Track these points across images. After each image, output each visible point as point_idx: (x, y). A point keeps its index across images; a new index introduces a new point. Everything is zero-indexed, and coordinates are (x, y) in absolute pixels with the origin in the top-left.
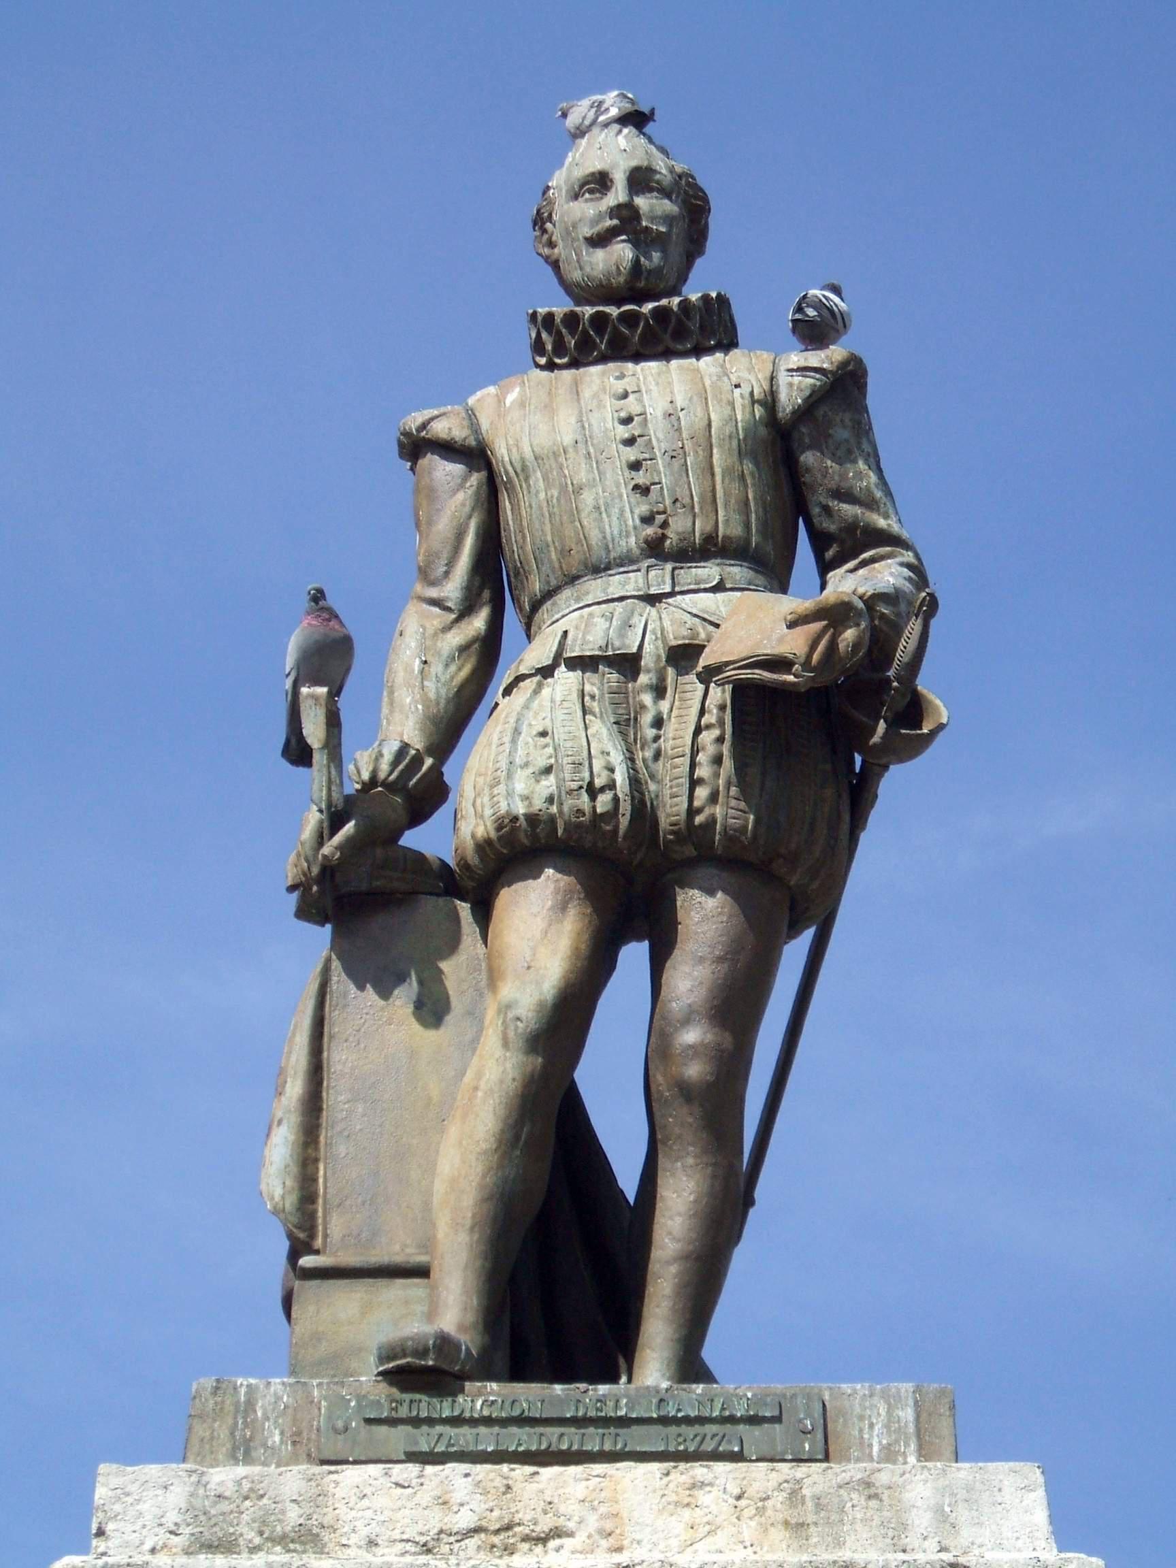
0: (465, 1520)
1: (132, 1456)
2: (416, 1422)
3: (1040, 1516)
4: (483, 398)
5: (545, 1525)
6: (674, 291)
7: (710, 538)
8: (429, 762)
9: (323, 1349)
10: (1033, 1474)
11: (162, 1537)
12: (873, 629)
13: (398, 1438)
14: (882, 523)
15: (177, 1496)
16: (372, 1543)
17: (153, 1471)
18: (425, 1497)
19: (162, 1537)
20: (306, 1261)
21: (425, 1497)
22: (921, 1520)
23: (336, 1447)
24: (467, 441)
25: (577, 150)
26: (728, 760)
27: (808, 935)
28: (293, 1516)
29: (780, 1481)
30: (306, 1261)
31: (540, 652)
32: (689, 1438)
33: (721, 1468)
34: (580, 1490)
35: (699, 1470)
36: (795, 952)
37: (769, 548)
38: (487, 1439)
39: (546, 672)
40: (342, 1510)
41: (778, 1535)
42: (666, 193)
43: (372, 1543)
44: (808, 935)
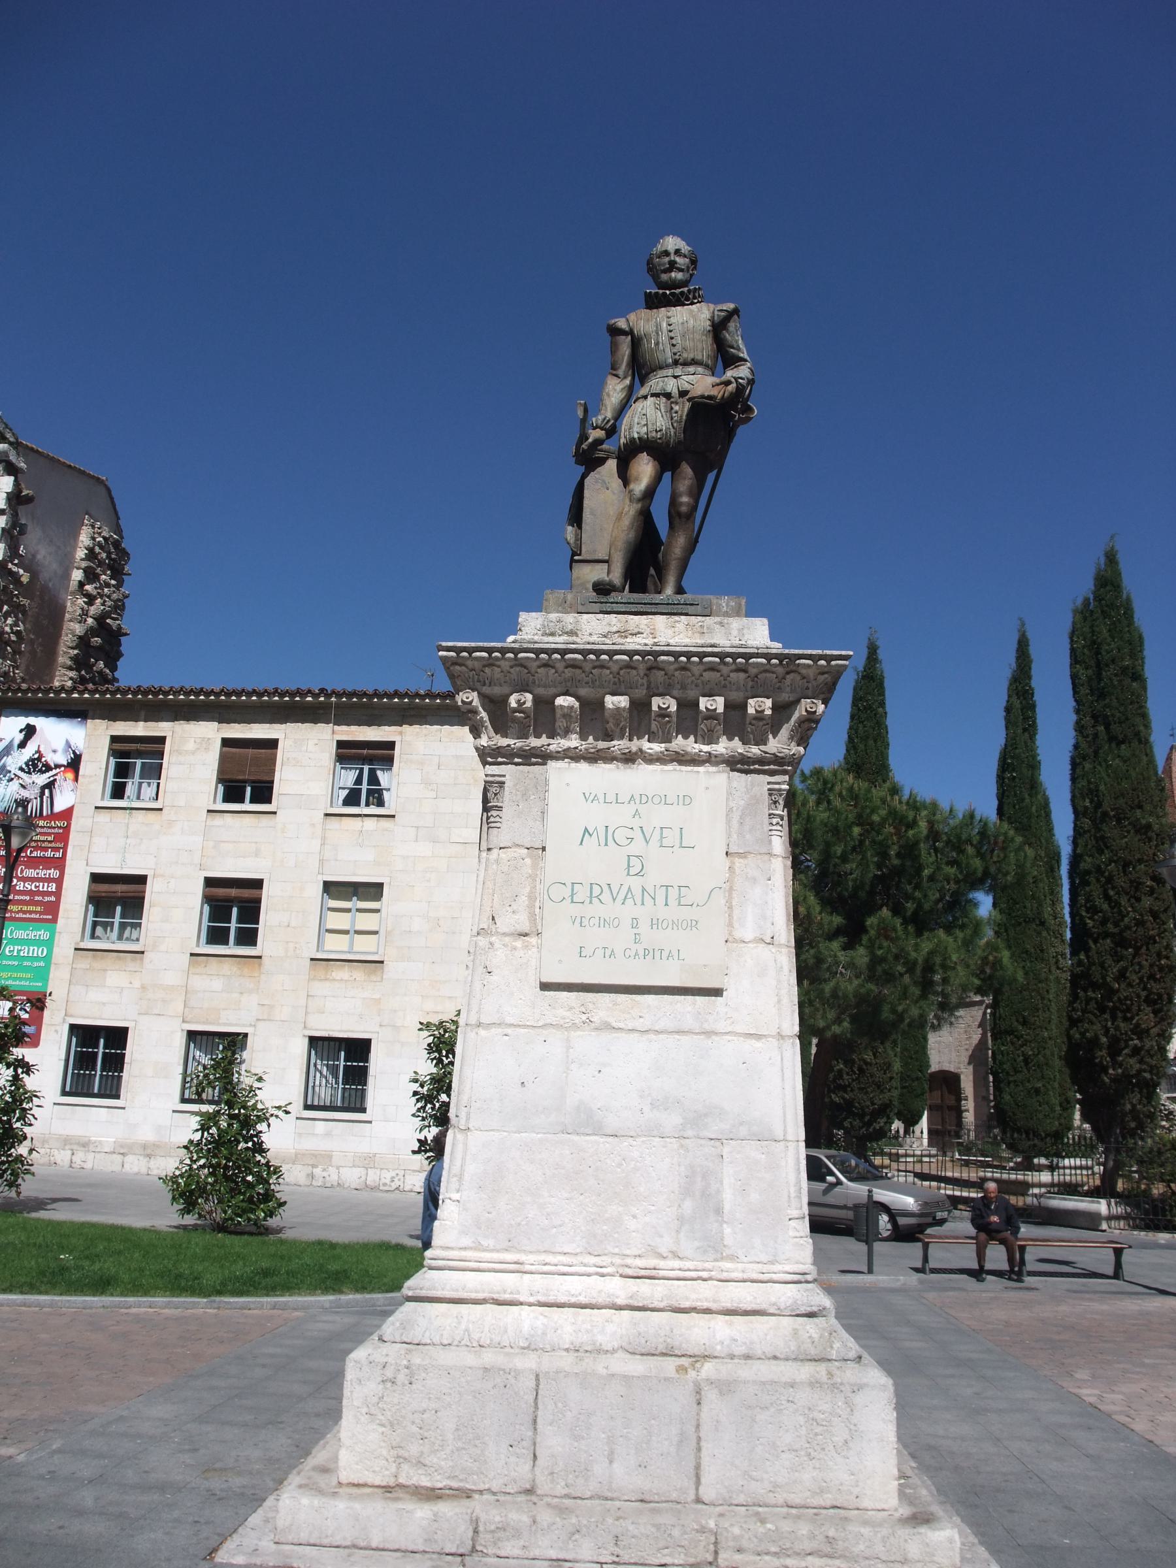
0: (615, 629)
1: (529, 611)
2: (602, 603)
3: (767, 632)
4: (632, 317)
5: (636, 630)
6: (687, 286)
7: (693, 360)
8: (612, 421)
9: (579, 582)
10: (765, 621)
11: (536, 631)
12: (737, 387)
13: (597, 607)
14: (742, 355)
15: (540, 621)
16: (591, 634)
17: (534, 614)
18: (604, 623)
19: (536, 631)
20: (576, 558)
21: (604, 623)
22: (735, 633)
23: (581, 609)
24: (27, 1177)
25: (606, 410)
26: (1137, 1308)
27: (715, 472)
28: (570, 627)
29: (880, 1556)
30: (576, 558)
31: (644, 391)
32: (675, 609)
33: (683, 617)
34: (645, 622)
35: (676, 618)
36: (711, 477)
37: (710, 362)
38: (622, 608)
39: (645, 397)
40: (583, 626)
41: (697, 635)
42: (685, 256)
43: (591, 634)
44: (715, 472)
